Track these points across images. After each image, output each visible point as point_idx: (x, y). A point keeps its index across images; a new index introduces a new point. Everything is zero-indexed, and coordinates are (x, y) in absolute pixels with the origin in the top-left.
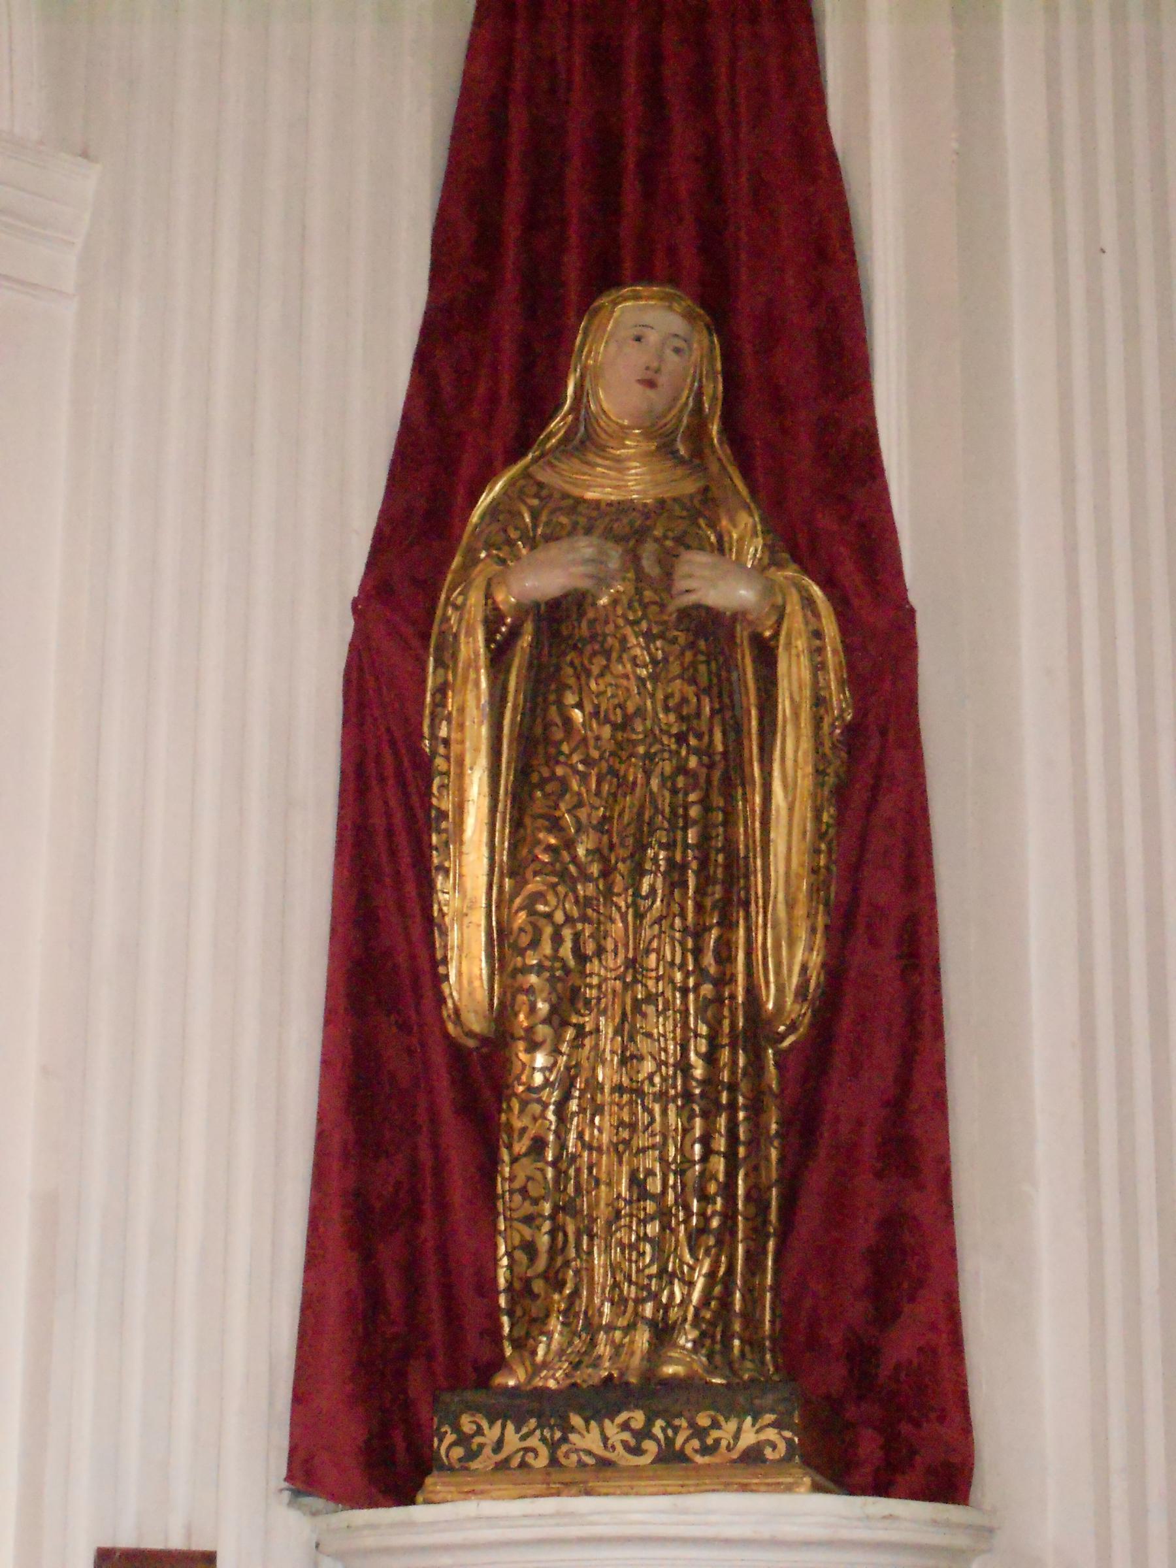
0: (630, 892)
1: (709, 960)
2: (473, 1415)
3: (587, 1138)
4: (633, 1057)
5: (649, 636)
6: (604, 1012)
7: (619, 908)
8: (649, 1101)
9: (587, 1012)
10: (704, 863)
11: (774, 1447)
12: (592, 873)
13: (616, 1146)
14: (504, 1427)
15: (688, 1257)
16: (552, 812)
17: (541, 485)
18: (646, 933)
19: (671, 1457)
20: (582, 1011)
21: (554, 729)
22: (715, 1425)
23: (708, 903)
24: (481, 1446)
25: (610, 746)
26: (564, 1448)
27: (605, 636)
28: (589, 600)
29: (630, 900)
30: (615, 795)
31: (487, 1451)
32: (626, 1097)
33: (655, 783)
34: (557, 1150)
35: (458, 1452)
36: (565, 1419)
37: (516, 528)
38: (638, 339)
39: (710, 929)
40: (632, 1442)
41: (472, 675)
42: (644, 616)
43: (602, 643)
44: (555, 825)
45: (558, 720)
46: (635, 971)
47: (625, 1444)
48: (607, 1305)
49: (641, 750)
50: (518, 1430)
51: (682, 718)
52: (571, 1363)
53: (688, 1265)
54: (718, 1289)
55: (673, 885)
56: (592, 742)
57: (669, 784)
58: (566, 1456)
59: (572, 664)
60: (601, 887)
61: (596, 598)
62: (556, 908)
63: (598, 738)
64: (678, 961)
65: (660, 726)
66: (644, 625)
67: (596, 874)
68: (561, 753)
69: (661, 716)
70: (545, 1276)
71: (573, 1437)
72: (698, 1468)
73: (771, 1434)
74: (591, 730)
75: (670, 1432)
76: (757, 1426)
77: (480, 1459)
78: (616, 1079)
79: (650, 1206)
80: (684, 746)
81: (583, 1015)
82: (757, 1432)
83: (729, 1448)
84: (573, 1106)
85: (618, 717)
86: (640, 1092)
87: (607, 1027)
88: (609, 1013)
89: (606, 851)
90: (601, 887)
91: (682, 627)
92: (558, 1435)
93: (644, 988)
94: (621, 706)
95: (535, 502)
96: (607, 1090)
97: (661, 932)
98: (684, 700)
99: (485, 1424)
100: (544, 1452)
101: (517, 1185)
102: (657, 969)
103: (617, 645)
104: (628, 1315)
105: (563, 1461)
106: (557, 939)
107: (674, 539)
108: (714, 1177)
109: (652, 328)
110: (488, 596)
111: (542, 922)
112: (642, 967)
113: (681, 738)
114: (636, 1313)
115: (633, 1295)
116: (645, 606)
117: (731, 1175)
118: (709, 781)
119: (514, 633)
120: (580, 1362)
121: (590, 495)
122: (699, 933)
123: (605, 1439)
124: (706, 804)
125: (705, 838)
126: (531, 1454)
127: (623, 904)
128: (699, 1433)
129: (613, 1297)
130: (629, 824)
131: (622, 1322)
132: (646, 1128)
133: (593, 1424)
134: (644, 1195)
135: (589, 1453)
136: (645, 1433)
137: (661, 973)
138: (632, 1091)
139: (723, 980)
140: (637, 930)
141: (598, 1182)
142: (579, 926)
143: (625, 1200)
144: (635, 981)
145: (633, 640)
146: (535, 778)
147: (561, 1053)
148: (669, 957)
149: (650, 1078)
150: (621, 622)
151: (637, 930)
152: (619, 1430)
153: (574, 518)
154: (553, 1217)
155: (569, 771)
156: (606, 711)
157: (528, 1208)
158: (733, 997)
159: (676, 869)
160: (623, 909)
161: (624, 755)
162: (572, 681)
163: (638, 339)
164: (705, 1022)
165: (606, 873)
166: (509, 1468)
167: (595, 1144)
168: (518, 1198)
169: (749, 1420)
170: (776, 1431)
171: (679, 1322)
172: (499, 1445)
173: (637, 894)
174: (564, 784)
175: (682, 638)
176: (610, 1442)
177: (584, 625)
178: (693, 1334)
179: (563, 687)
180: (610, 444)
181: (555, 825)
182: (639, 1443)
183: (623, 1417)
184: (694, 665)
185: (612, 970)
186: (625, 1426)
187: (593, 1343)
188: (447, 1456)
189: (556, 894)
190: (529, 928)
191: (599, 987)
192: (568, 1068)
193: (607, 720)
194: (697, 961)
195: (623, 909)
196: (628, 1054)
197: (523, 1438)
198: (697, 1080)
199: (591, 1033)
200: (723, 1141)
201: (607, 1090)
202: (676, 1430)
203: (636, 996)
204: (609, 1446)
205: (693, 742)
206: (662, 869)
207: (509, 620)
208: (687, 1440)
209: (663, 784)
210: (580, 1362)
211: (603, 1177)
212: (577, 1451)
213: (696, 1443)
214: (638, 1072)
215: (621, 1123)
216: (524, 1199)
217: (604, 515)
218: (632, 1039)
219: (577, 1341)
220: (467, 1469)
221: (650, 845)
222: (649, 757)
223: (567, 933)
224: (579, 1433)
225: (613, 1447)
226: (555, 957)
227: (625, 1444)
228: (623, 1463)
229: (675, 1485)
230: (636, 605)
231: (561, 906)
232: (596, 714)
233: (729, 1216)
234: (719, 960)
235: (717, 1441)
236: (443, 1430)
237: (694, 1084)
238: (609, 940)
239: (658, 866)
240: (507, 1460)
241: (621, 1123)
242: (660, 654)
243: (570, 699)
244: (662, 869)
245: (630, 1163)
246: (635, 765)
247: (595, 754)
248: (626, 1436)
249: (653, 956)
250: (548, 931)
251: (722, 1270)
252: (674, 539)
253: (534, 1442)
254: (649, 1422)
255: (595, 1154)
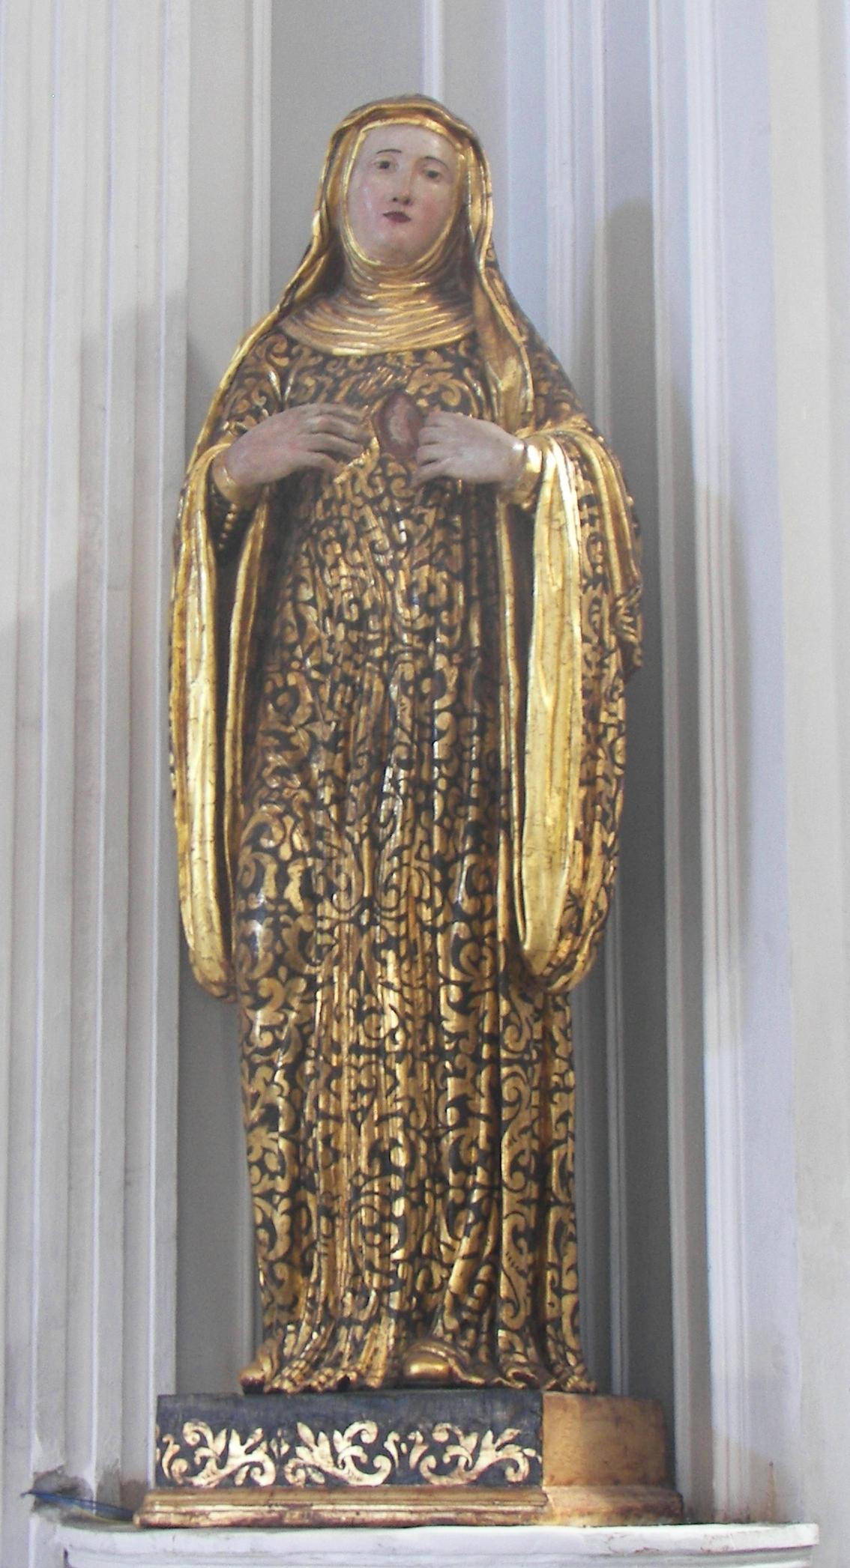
0: (365, 820)
1: (460, 895)
2: (196, 1424)
3: (321, 1105)
4: (372, 1010)
5: (392, 518)
6: (337, 961)
7: (351, 839)
8: (391, 1062)
9: (318, 961)
10: (454, 781)
11: (516, 1467)
12: (323, 800)
13: (353, 1114)
14: (229, 1436)
15: (445, 1237)
16: (283, 728)
17: (292, 342)
18: (385, 867)
19: (404, 1477)
20: (313, 960)
21: (289, 629)
22: (454, 1440)
23: (461, 826)
24: (205, 1460)
25: (343, 650)
26: (291, 1464)
27: (341, 518)
28: (326, 477)
29: (364, 829)
30: (350, 707)
31: (211, 1465)
32: (363, 1059)
33: (394, 690)
34: (293, 1118)
35: (181, 1465)
36: (294, 1430)
37: (262, 394)
38: (385, 165)
39: (460, 857)
40: (364, 1458)
41: (194, 574)
42: (388, 492)
43: (338, 528)
44: (285, 743)
45: (292, 619)
46: (372, 911)
47: (355, 1459)
48: (349, 1295)
49: (378, 652)
50: (243, 1443)
51: (428, 610)
52: (308, 1362)
53: (446, 1245)
54: (483, 1273)
55: (418, 809)
56: (326, 644)
57: (411, 691)
58: (294, 1472)
59: (307, 554)
60: (333, 815)
61: (332, 476)
62: (282, 842)
63: (332, 639)
64: (427, 894)
65: (400, 623)
66: (386, 504)
67: (327, 801)
68: (294, 658)
69: (401, 610)
70: (286, 1258)
71: (301, 1451)
72: (432, 1491)
73: (514, 1452)
74: (324, 629)
75: (404, 1447)
76: (499, 1442)
77: (203, 1474)
78: (352, 1037)
79: (396, 1182)
80: (432, 643)
81: (314, 965)
82: (498, 1449)
83: (467, 1468)
84: (309, 1067)
85: (353, 614)
86: (380, 1052)
87: (342, 979)
88: (344, 960)
89: (340, 772)
90: (333, 815)
91: (430, 503)
92: (285, 1448)
93: (383, 932)
94: (358, 601)
95: (284, 362)
96: (345, 1049)
97: (401, 864)
98: (432, 589)
99: (209, 1435)
100: (269, 1466)
101: (254, 1157)
102: (398, 907)
103: (353, 532)
104: (369, 1308)
105: (290, 1478)
106: (282, 879)
107: (428, 398)
108: (474, 1143)
109: (400, 152)
110: (209, 481)
111: (266, 859)
112: (380, 906)
113: (427, 635)
114: (380, 1302)
115: (375, 1284)
116: (388, 480)
117: (494, 1140)
118: (461, 684)
119: (245, 519)
120: (320, 1360)
121: (338, 351)
122: (445, 864)
123: (334, 1453)
124: (458, 711)
125: (457, 749)
126: (257, 1470)
127: (356, 836)
128: (436, 1449)
129: (355, 1284)
130: (363, 741)
131: (364, 1316)
132: (389, 1092)
133: (322, 1435)
134: (389, 1168)
135: (319, 1469)
136: (376, 1449)
137: (403, 911)
138: (369, 1051)
139: (482, 915)
140: (375, 865)
141: (336, 1155)
142: (310, 861)
143: (364, 1176)
144: (372, 922)
145: (372, 522)
146: (269, 687)
147: (292, 1009)
148: (416, 892)
149: (392, 1033)
150: (359, 501)
151: (375, 865)
152: (350, 1443)
153: (320, 378)
154: (290, 1194)
155: (302, 678)
156: (340, 607)
157: (266, 1184)
158: (493, 934)
159: (421, 787)
160: (357, 840)
161: (360, 658)
162: (306, 574)
163: (385, 165)
164: (458, 966)
165: (339, 799)
166: (234, 1485)
167: (332, 1111)
168: (256, 1172)
169: (490, 1435)
170: (518, 1448)
171: (438, 1310)
172: (223, 1459)
173: (374, 817)
174: (295, 693)
175: (430, 517)
176: (340, 1458)
177: (320, 505)
178: (452, 1324)
179: (299, 580)
180: (365, 289)
181: (285, 743)
182: (371, 1459)
183: (356, 1427)
184: (445, 546)
185: (345, 912)
186: (356, 1440)
187: (334, 1339)
188: (169, 1468)
189: (284, 827)
190: (253, 867)
191: (331, 931)
192: (299, 1026)
193: (339, 619)
194: (445, 896)
195: (357, 840)
196: (365, 1008)
197: (249, 1451)
198: (448, 1034)
199: (322, 986)
200: (483, 1102)
201: (345, 1049)
202: (411, 1445)
203: (375, 941)
204: (339, 1462)
205: (441, 639)
206: (402, 791)
207: (234, 507)
208: (421, 1459)
209: (403, 689)
210: (320, 1360)
211: (343, 1147)
212: (304, 1467)
213: (431, 1461)
214: (378, 1029)
215: (360, 1088)
216: (262, 1175)
217: (349, 373)
218: (369, 990)
219: (315, 1335)
220: (191, 1484)
221: (388, 764)
222: (390, 658)
223: (295, 871)
224: (307, 1446)
225: (344, 1464)
226: (280, 899)
227: (355, 1459)
228: (353, 1483)
229: (405, 1511)
230: (378, 480)
231: (287, 839)
232: (328, 613)
233: (494, 1187)
234: (472, 891)
235: (455, 1459)
236: (165, 1440)
237: (446, 1038)
238: (343, 877)
239: (397, 788)
240: (232, 1476)
241: (360, 1088)
242: (404, 537)
243: (306, 593)
244: (402, 791)
245: (369, 1132)
246: (370, 670)
247: (329, 659)
248: (358, 1451)
249: (393, 893)
250: (272, 868)
251: (488, 1250)
252: (429, 398)
253: (259, 1455)
254: (382, 1436)
255: (332, 1124)
